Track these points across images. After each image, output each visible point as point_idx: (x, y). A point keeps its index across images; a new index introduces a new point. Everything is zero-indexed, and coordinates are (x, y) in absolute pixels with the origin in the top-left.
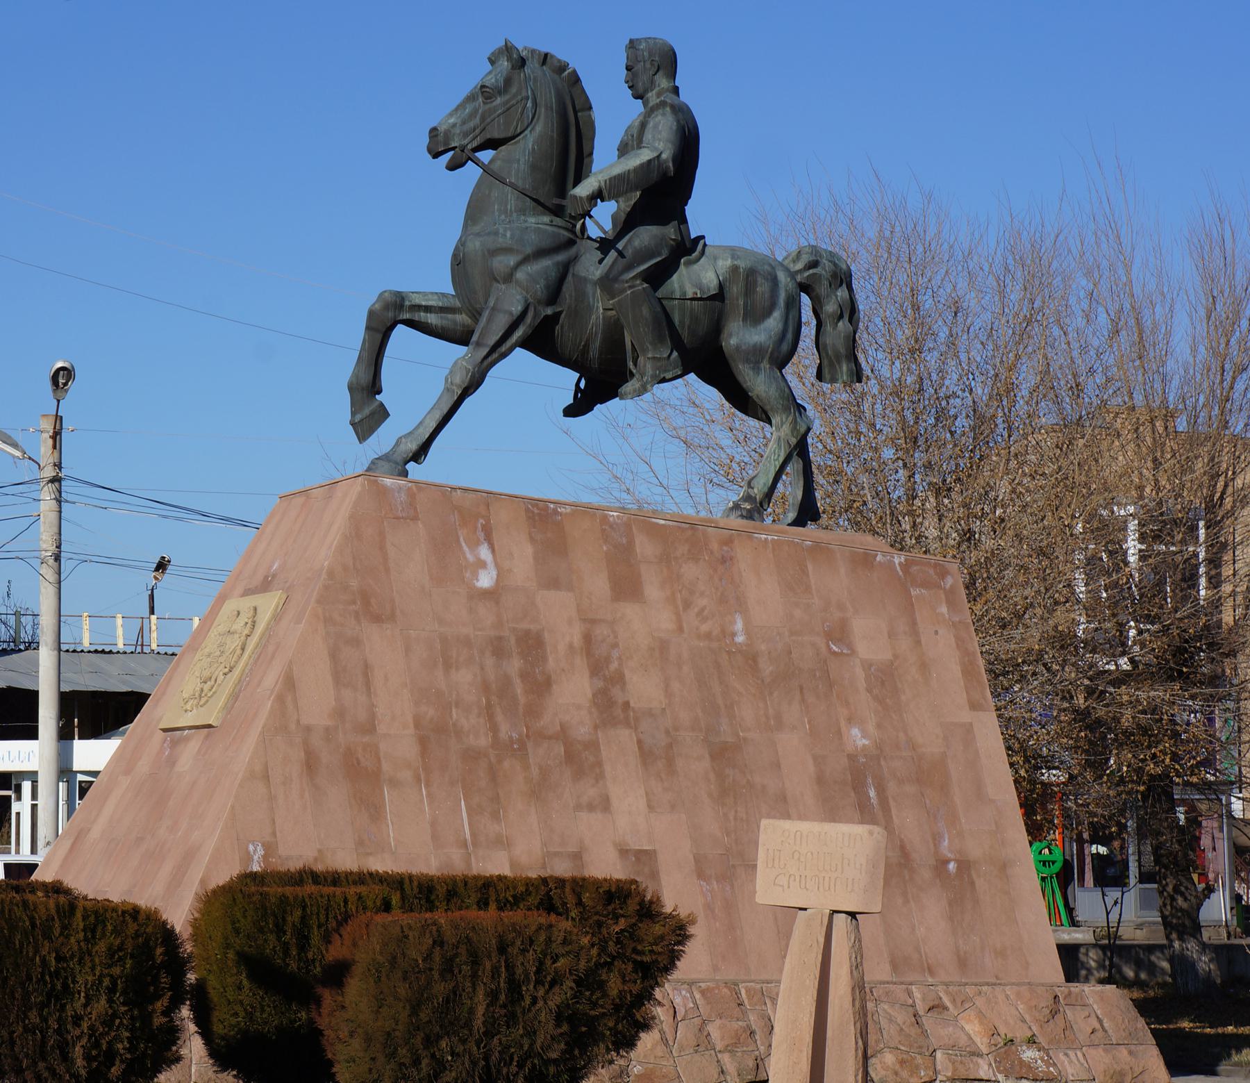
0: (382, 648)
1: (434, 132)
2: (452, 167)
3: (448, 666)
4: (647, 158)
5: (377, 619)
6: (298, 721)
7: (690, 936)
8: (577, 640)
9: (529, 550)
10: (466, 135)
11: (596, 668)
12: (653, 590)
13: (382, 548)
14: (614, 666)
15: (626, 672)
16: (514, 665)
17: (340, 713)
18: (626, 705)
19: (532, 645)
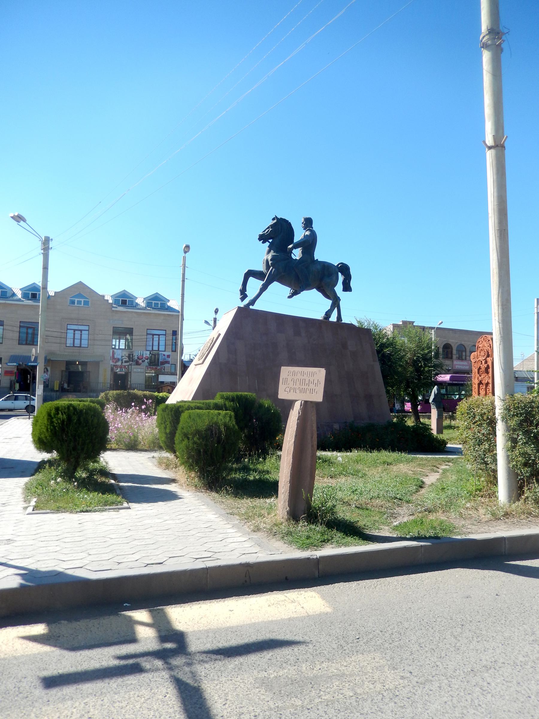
2: (263, 243)
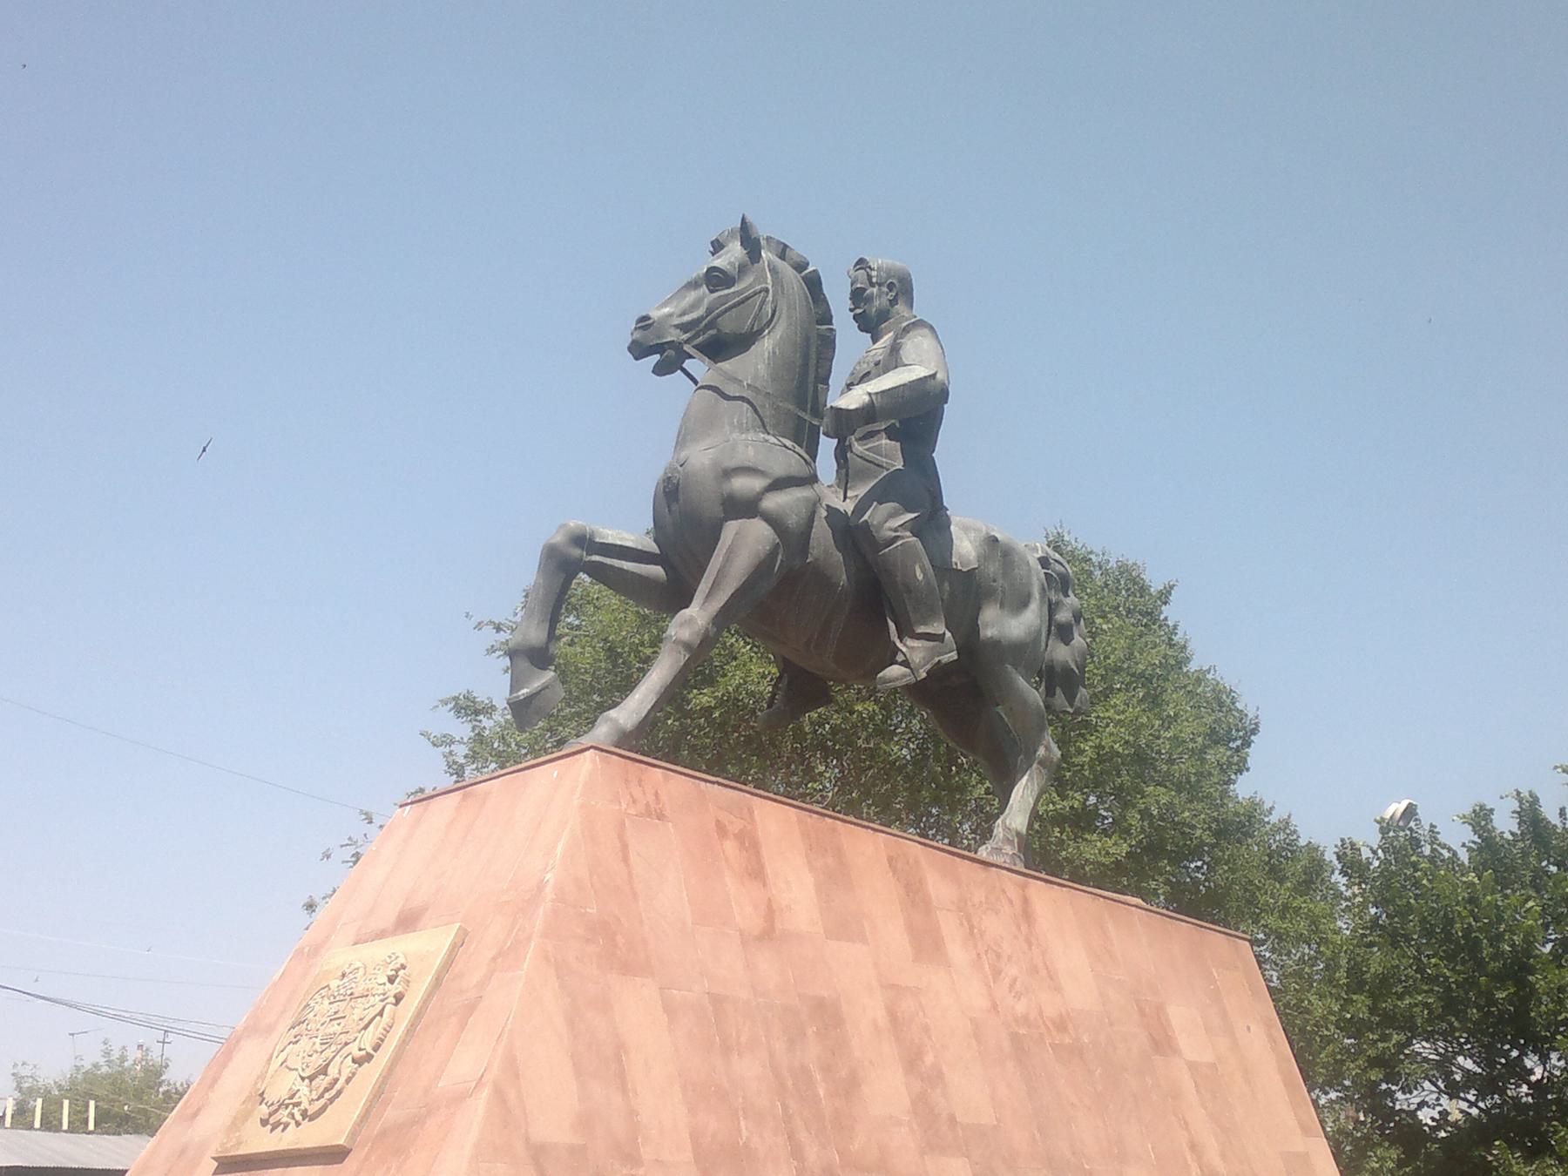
0: (637, 1011)
1: (644, 322)
2: (660, 370)
3: (727, 1050)
4: (923, 374)
5: (628, 969)
6: (527, 1140)
7: (1287, 823)
8: (881, 1015)
9: (809, 879)
10: (684, 328)
11: (911, 1062)
12: (956, 950)
13: (626, 859)
14: (929, 1059)
15: (945, 1069)
16: (812, 1052)
17: (585, 1122)
18: (952, 1120)
19: (827, 1016)
